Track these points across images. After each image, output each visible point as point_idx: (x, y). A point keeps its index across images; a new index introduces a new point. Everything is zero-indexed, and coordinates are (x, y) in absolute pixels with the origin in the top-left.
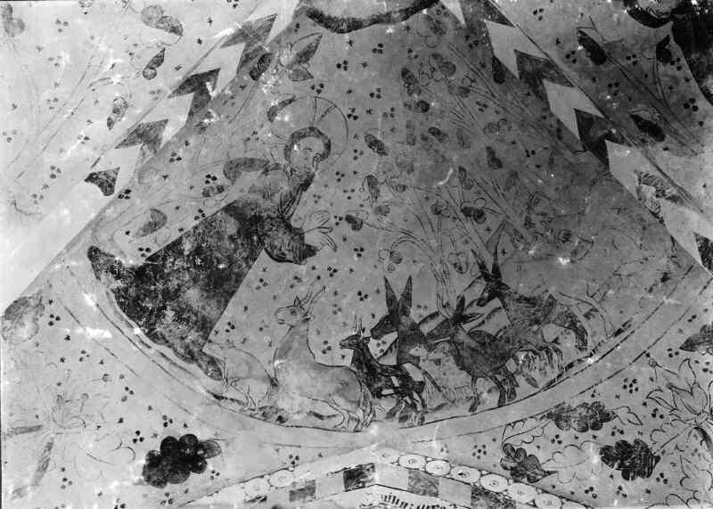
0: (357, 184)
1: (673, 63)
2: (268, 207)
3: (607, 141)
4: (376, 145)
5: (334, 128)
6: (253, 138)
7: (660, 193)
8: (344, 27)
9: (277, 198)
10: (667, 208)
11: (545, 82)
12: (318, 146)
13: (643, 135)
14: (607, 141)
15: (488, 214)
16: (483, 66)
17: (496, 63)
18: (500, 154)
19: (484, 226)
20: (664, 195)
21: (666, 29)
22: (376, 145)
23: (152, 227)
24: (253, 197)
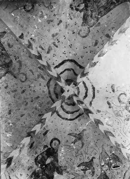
0: (15, 88)
2: (11, 69)
3: (30, 137)
4: (23, 91)
5: (27, 83)
6: (26, 67)
7: (21, 148)
8: (48, 85)
9: (13, 71)
10: (18, 150)
11: (41, 124)
12: (23, 80)
13: (31, 144)
14: (30, 137)
15: (10, 115)
16: (42, 112)
17: (43, 115)
18: (24, 117)
19: (7, 115)
20: (21, 149)
21: (49, 147)
22: (23, 91)
23: (9, 45)
24: (13, 66)
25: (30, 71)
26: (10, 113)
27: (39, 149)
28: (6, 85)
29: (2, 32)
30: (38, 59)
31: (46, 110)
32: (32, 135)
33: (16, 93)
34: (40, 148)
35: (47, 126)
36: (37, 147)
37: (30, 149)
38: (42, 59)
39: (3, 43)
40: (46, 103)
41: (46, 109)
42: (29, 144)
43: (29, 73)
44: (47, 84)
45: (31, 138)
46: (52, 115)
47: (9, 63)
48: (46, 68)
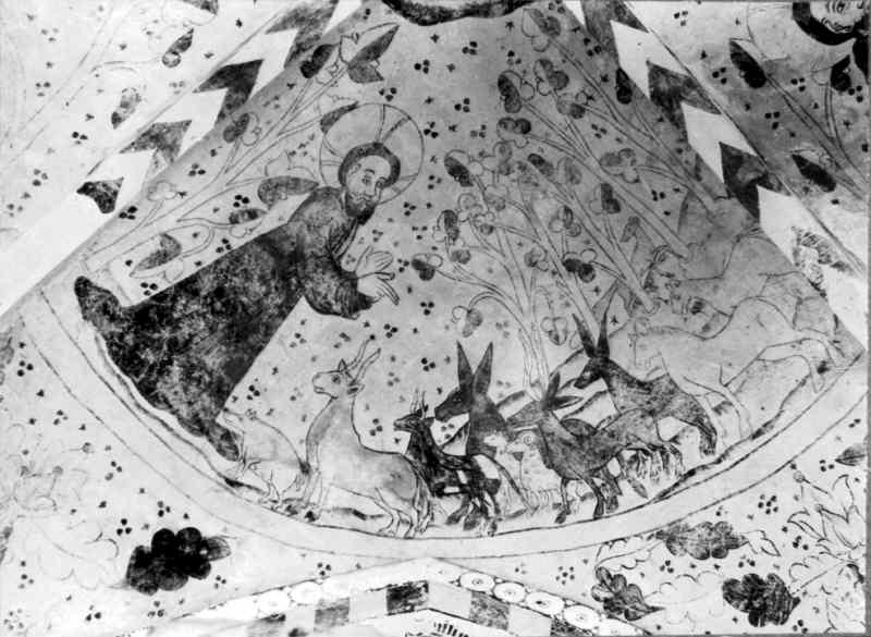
1: (851, 92)
2: (314, 242)
3: (760, 189)
4: (459, 172)
5: (406, 146)
7: (824, 259)
9: (325, 232)
10: (830, 277)
14: (760, 189)
17: (621, 76)
19: (593, 284)
21: (846, 48)
23: (161, 257)
25: (333, 130)
26: (585, 271)
27: (847, 124)
28: (410, 270)
29: (81, 303)
30: (249, 91)
31: (597, 50)
32: (751, 176)
33: (462, 216)
34: (841, 114)
35: (704, 55)
36: (832, 140)
37: (839, 187)
38: (256, 64)
39: (146, 293)
40: (614, 569)
41: (591, 47)
42: (807, 190)
43: (348, 133)
44: (424, 23)
45: (770, 187)
46: (634, 23)
47: (276, 253)
48: (312, 34)
